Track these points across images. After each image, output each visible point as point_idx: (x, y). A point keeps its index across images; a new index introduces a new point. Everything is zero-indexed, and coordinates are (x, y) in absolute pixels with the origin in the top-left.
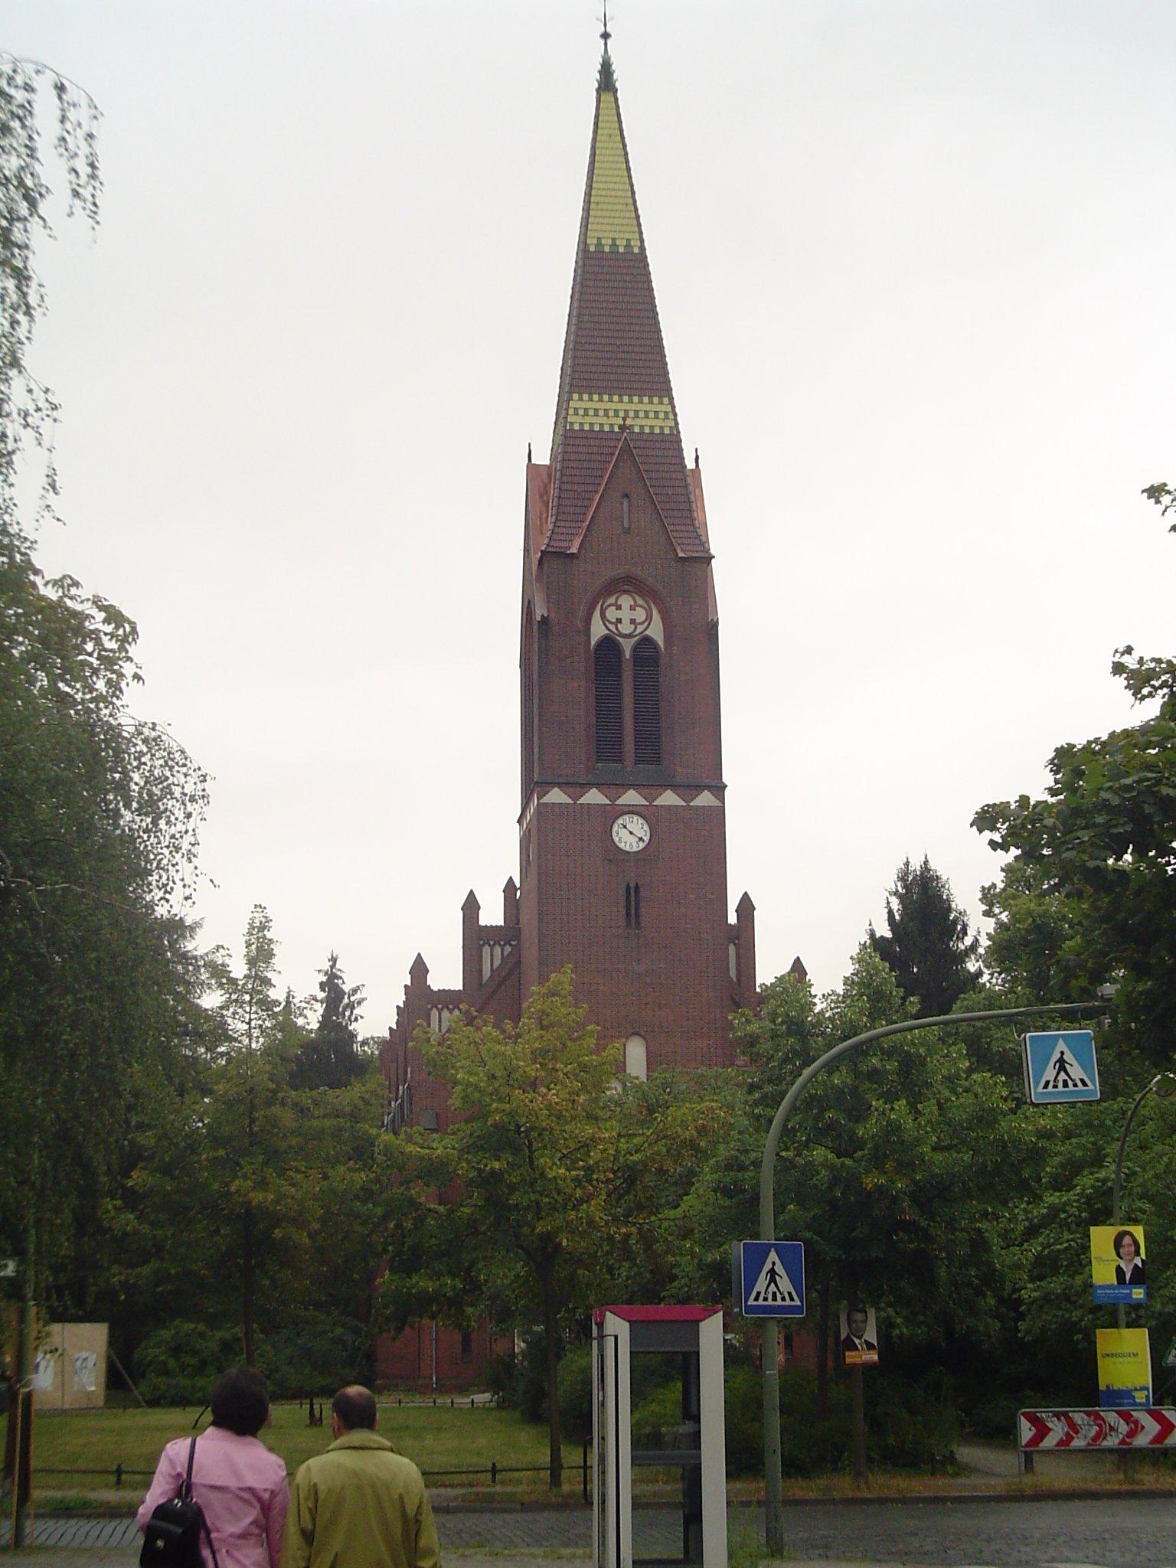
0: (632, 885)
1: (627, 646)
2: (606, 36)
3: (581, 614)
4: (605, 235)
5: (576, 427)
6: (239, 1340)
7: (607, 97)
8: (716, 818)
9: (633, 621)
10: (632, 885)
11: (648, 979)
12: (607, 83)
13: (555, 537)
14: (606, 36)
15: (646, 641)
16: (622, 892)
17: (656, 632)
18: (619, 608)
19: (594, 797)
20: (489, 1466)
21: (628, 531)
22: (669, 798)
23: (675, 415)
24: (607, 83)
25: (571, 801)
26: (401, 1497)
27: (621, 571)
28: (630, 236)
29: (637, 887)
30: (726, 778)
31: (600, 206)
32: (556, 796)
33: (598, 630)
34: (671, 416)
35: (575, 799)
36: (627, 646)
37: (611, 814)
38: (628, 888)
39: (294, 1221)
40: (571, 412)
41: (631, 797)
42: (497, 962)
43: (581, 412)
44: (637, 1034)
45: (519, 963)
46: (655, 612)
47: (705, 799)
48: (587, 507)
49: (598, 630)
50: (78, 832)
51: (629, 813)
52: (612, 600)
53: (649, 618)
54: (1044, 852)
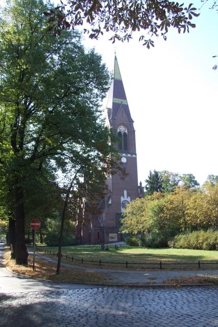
1: (123, 133)
6: (37, 233)
8: (135, 159)
12: (116, 59)
15: (125, 133)
17: (126, 132)
20: (72, 257)
22: (129, 155)
24: (116, 59)
26: (13, 271)
30: (137, 153)
33: (118, 131)
36: (123, 133)
41: (124, 155)
47: (134, 156)
49: (118, 131)
50: (80, 160)
54: (93, 141)
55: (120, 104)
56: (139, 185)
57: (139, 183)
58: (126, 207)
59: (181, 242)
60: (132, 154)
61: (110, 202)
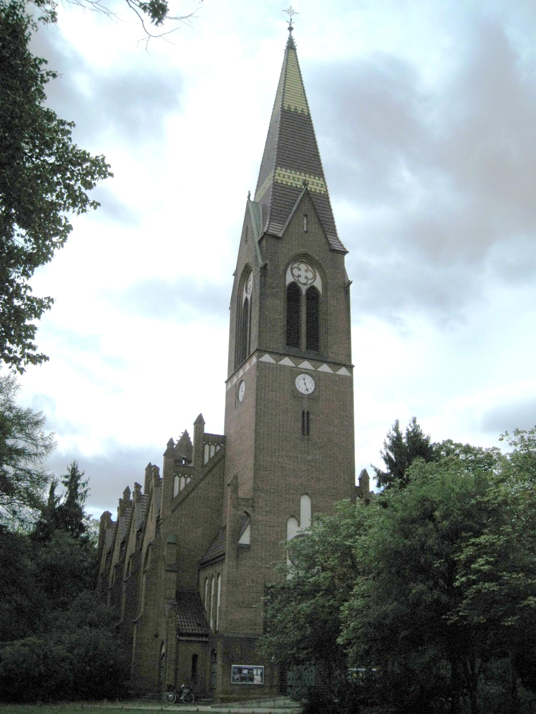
0: (306, 412)
1: (304, 289)
2: (290, 29)
3: (282, 268)
4: (293, 104)
5: (279, 182)
7: (291, 51)
8: (349, 382)
9: (306, 278)
10: (306, 412)
11: (313, 464)
12: (291, 47)
13: (270, 225)
14: (290, 29)
15: (312, 290)
16: (300, 414)
17: (318, 284)
18: (299, 269)
19: (287, 362)
21: (306, 232)
22: (325, 368)
23: (326, 186)
24: (291, 47)
25: (274, 362)
27: (302, 250)
28: (303, 107)
29: (308, 413)
30: (353, 362)
31: (289, 92)
32: (267, 358)
34: (324, 186)
35: (277, 361)
36: (304, 289)
37: (295, 372)
38: (303, 413)
39: (298, 585)
40: (277, 174)
41: (306, 365)
42: (212, 454)
43: (282, 176)
44: (306, 494)
45: (223, 457)
46: (318, 274)
47: (343, 371)
48: (286, 219)
49: (289, 279)
51: (306, 373)
52: (296, 265)
53: (315, 277)
55: (300, 190)
56: (357, 484)
57: (358, 475)
58: (160, 20)
59: (163, 680)
60: (336, 365)
61: (245, 539)
